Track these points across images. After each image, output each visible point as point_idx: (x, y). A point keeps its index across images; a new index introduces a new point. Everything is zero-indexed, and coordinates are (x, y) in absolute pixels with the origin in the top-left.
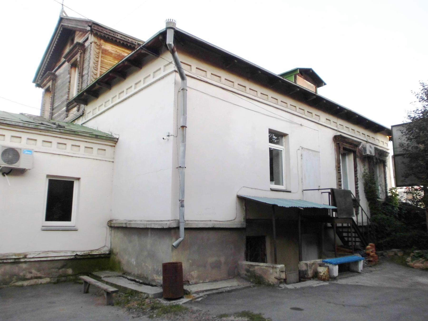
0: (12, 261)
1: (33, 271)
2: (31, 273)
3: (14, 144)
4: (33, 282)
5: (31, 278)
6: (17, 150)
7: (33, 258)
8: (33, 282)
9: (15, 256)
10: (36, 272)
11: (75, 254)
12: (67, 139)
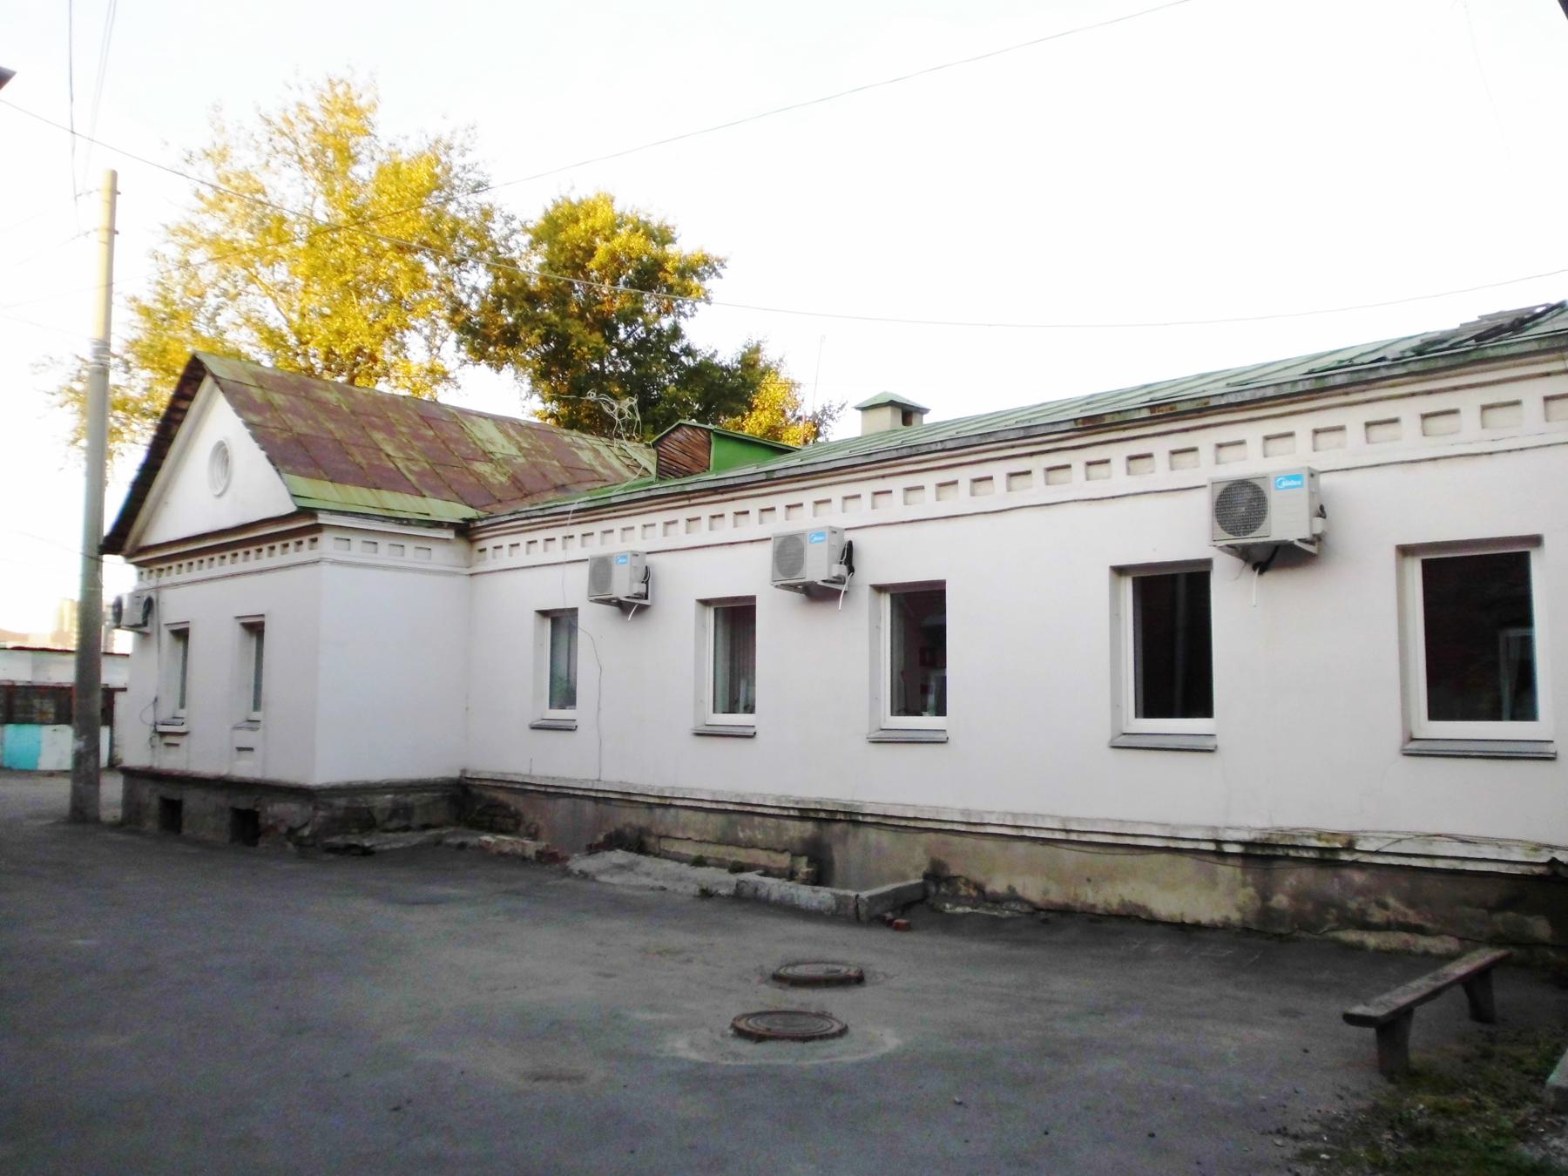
0: (1311, 854)
1: (1391, 901)
2: (1384, 906)
3: (1238, 467)
4: (1395, 940)
5: (1387, 927)
6: (1257, 482)
7: (1377, 853)
8: (1395, 940)
9: (1319, 839)
10: (1402, 908)
11: (1545, 859)
12: (1456, 388)
